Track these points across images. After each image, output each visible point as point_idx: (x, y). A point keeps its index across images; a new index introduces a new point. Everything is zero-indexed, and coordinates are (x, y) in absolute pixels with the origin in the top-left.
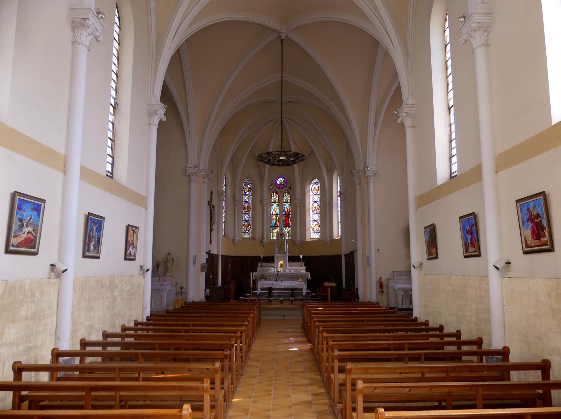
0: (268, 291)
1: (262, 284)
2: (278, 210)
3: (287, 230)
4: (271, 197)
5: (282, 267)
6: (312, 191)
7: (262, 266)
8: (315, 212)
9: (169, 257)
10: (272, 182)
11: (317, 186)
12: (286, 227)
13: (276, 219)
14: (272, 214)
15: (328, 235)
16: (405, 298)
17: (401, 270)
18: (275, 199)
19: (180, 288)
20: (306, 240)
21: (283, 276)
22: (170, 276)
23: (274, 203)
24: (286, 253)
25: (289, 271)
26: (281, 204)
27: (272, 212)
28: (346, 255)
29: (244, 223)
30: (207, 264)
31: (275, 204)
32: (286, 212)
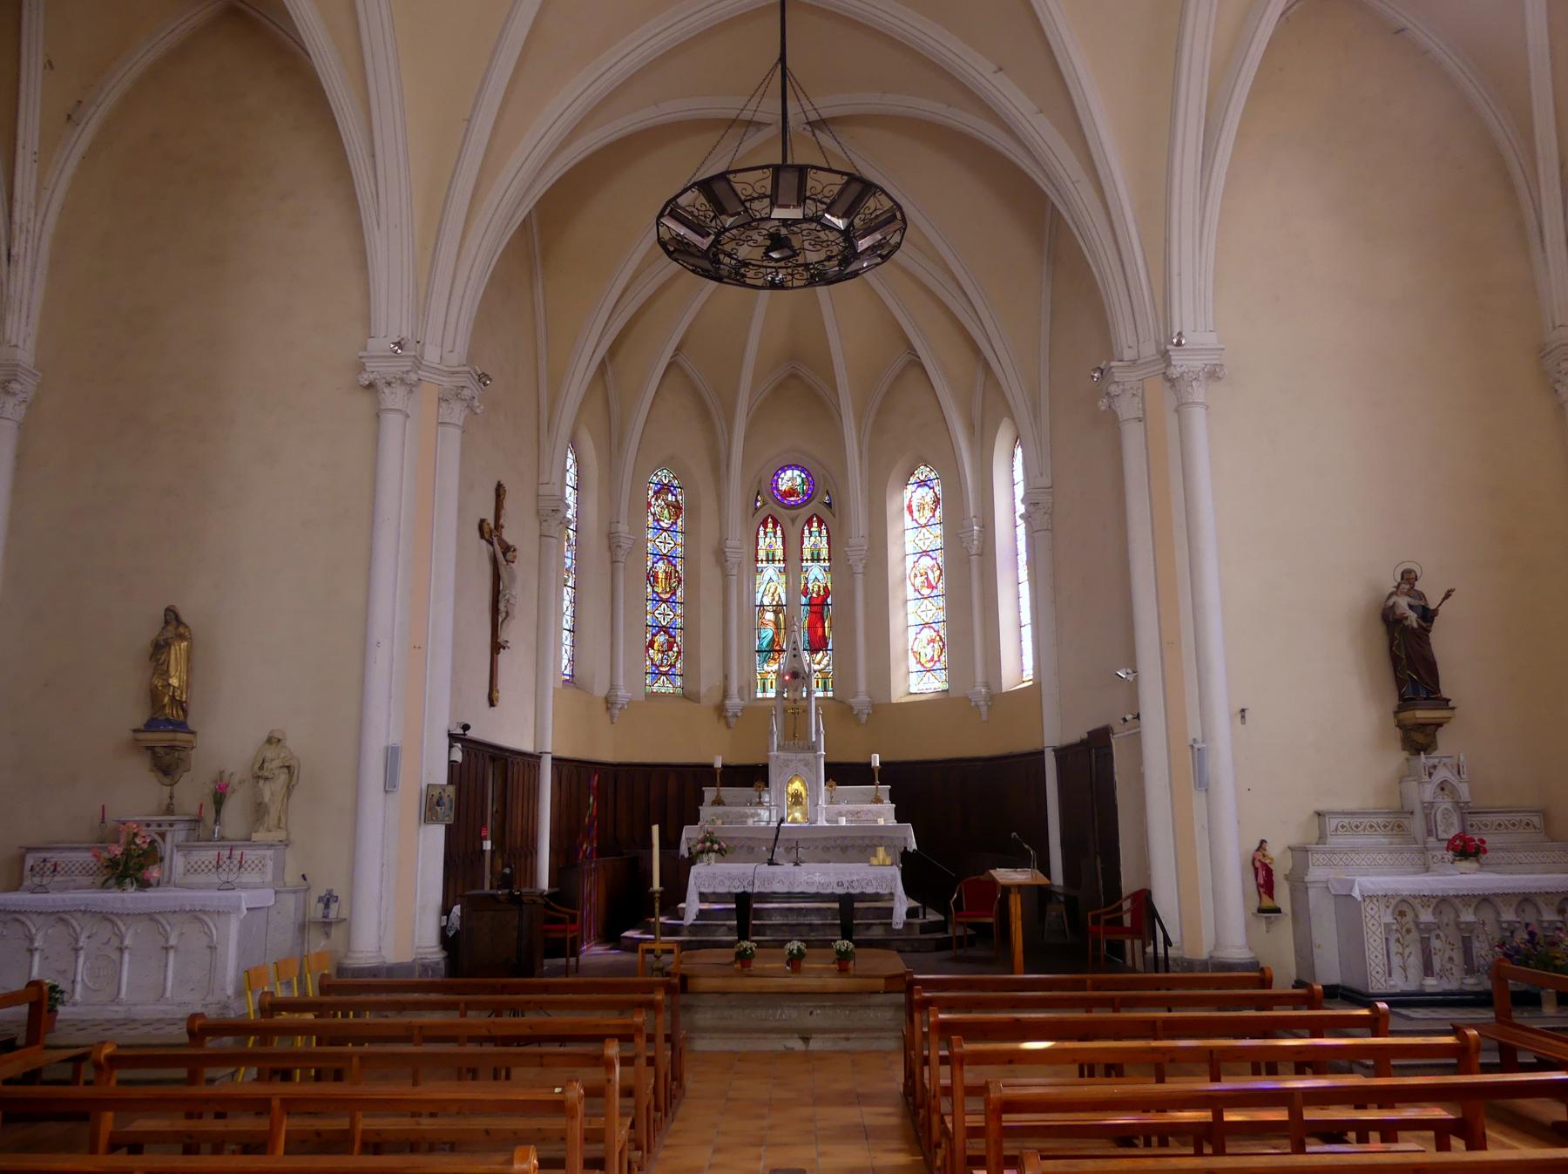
0: (734, 906)
1: (708, 877)
2: (781, 590)
3: (819, 663)
4: (757, 538)
5: (801, 804)
6: (911, 512)
7: (718, 802)
8: (926, 592)
9: (270, 753)
10: (760, 482)
11: (931, 494)
12: (814, 650)
13: (776, 623)
14: (762, 605)
15: (979, 678)
16: (1398, 940)
17: (1352, 805)
18: (770, 546)
19: (320, 900)
20: (894, 700)
21: (805, 840)
22: (270, 846)
23: (768, 561)
24: (813, 748)
25: (827, 821)
26: (792, 562)
27: (759, 596)
28: (1062, 753)
29: (654, 635)
30: (451, 790)
31: (771, 565)
32: (814, 595)
